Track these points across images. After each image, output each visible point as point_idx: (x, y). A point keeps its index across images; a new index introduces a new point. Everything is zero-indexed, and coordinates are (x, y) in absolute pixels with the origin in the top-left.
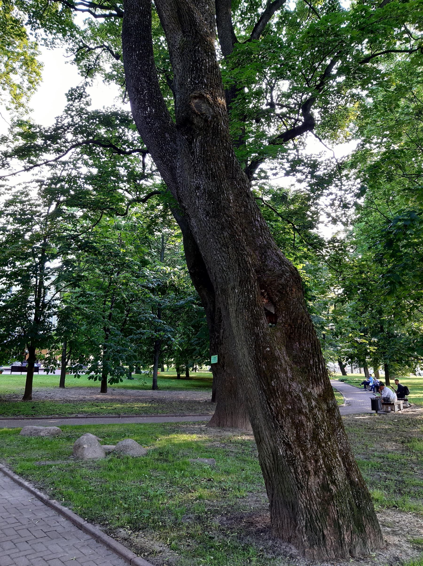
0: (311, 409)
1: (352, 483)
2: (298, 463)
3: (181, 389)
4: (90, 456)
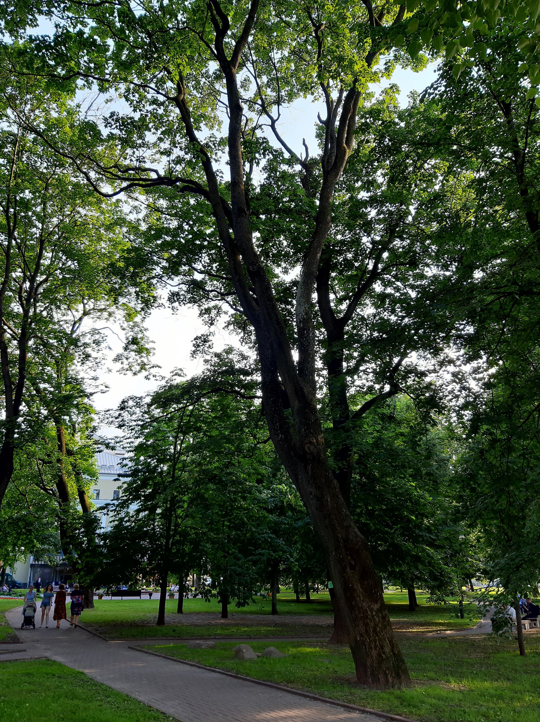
0: (373, 616)
1: (394, 654)
3: (302, 614)
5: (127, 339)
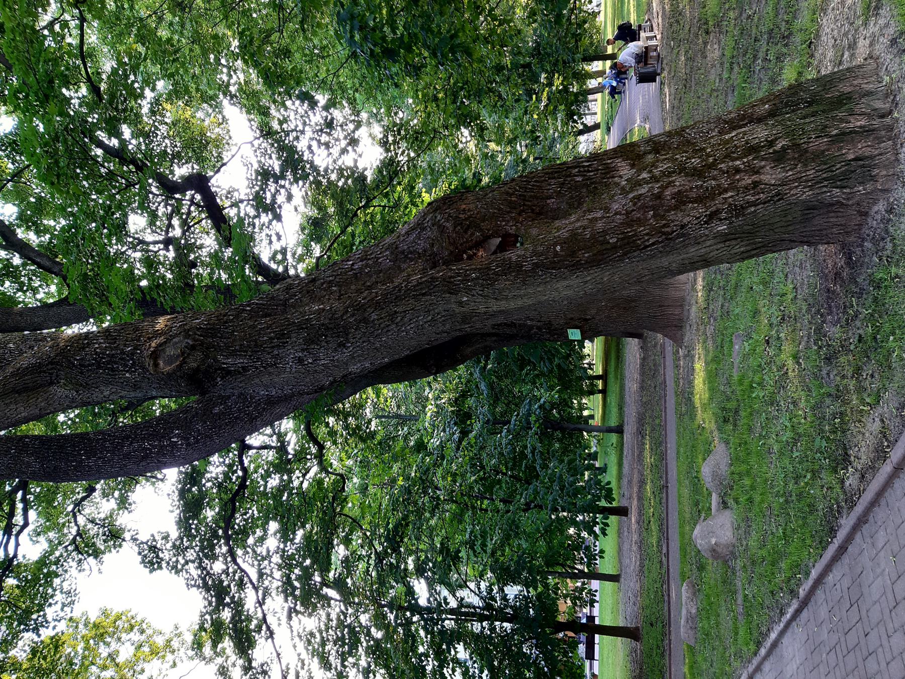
1: (772, 114)
2: (740, 200)
3: (622, 388)
5: (192, 658)
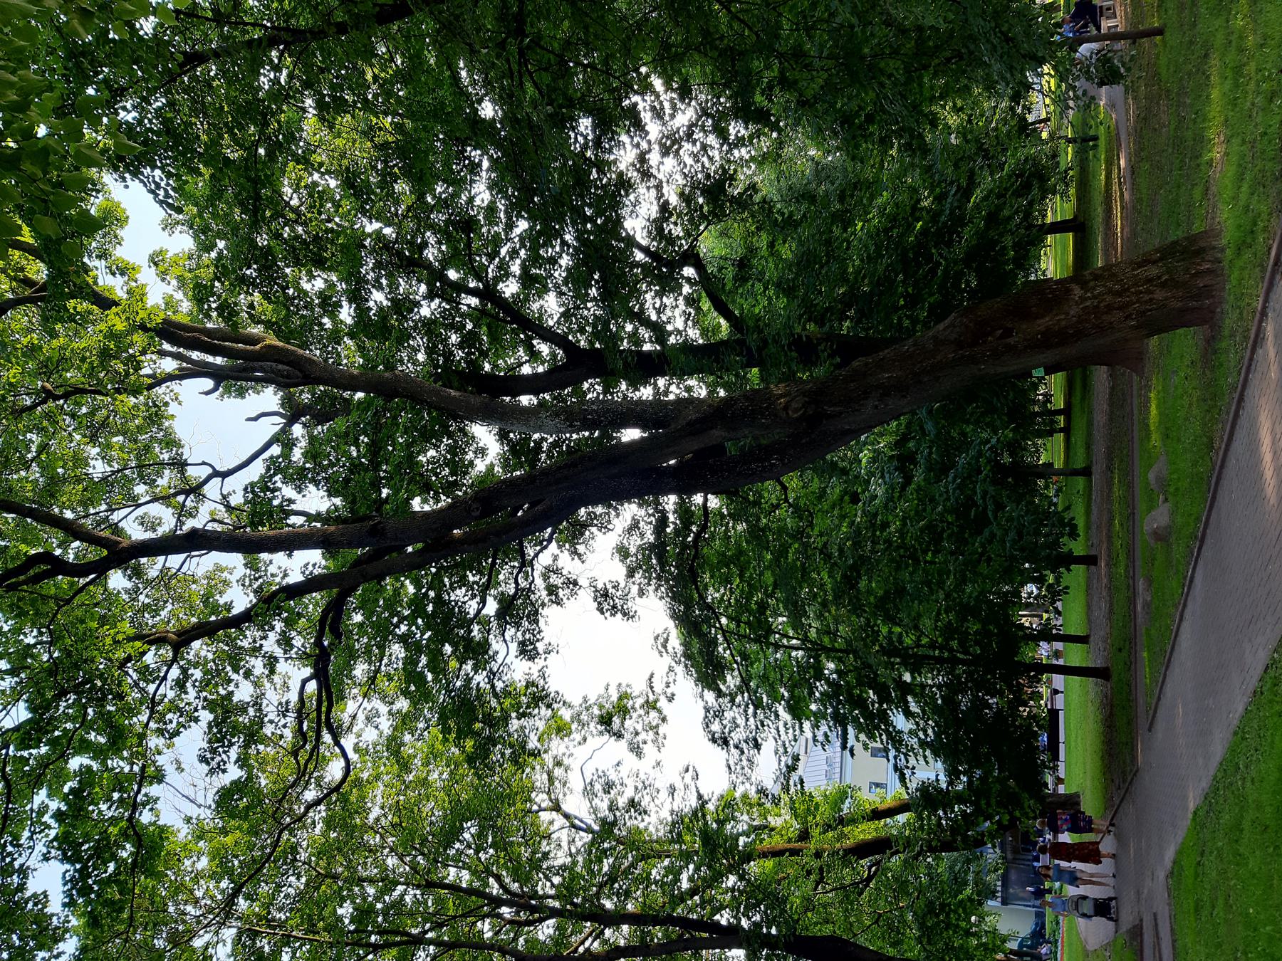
0: (1094, 297)
1: (1161, 259)
2: (1143, 308)
3: (1090, 423)
4: (1167, 519)
5: (601, 733)
